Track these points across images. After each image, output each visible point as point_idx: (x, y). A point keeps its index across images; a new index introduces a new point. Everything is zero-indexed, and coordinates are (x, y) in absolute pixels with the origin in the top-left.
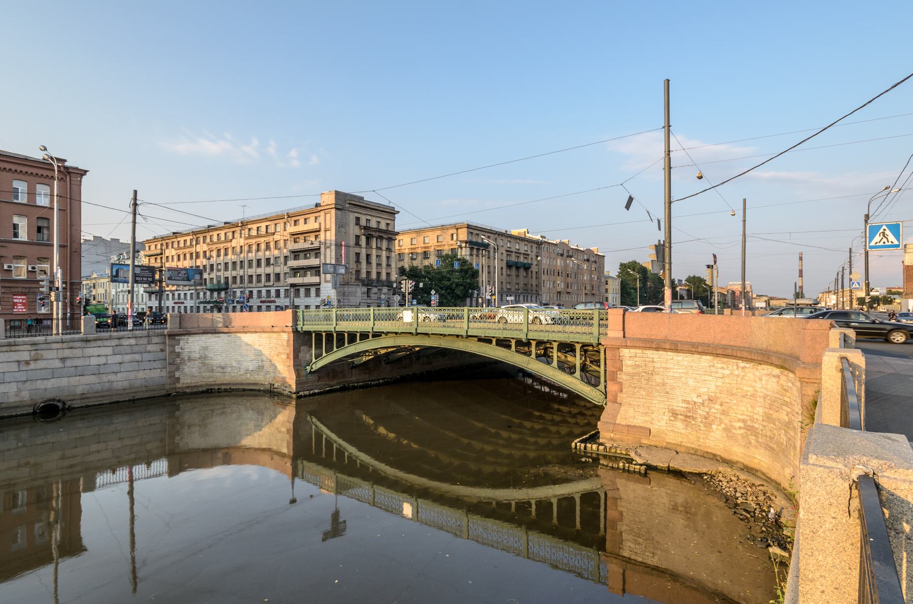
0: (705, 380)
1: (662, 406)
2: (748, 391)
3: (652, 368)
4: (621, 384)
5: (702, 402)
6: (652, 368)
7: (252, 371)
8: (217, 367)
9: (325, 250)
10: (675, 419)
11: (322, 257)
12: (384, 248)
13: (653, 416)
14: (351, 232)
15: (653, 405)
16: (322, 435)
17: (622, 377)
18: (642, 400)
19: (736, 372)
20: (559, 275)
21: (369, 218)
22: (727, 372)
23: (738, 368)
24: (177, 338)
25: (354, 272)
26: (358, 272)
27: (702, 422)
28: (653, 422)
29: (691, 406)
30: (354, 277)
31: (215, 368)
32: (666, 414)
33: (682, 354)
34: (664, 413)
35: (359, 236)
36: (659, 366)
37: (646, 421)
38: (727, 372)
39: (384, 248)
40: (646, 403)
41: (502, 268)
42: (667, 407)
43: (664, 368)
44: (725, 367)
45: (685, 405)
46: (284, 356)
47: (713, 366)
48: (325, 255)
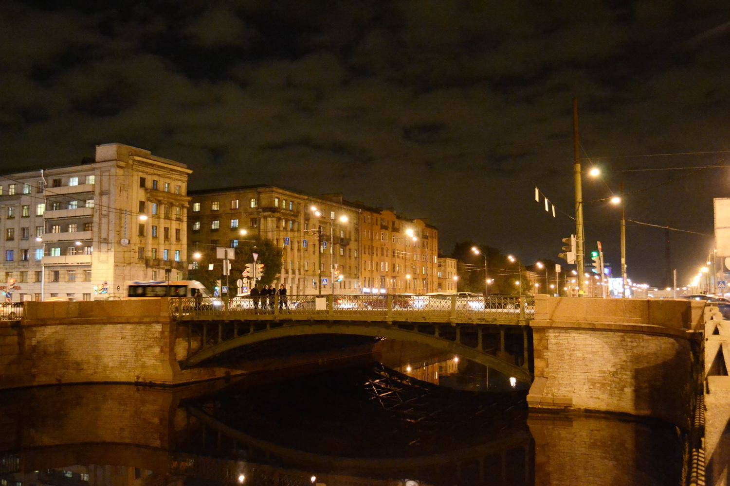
0: (618, 353)
1: (583, 377)
2: (652, 358)
3: (574, 345)
4: (547, 360)
5: (615, 370)
6: (574, 345)
7: (112, 367)
8: (72, 363)
9: (100, 219)
10: (593, 387)
11: (95, 229)
12: (174, 217)
13: (575, 386)
14: (134, 197)
15: (575, 377)
16: (484, 349)
17: (547, 354)
18: (565, 373)
19: (642, 344)
20: (365, 253)
21: (156, 178)
22: (635, 344)
23: (643, 341)
24: (34, 329)
25: (137, 250)
26: (142, 250)
27: (615, 387)
28: (575, 391)
29: (607, 375)
30: (136, 255)
31: (70, 364)
32: (586, 384)
33: (598, 332)
34: (584, 383)
35: (144, 202)
36: (583, 341)
37: (569, 392)
38: (635, 344)
39: (174, 217)
40: (569, 376)
41: (314, 245)
42: (586, 377)
43: (583, 345)
44: (633, 340)
45: (602, 375)
46: (157, 350)
47: (624, 341)
48: (100, 224)
